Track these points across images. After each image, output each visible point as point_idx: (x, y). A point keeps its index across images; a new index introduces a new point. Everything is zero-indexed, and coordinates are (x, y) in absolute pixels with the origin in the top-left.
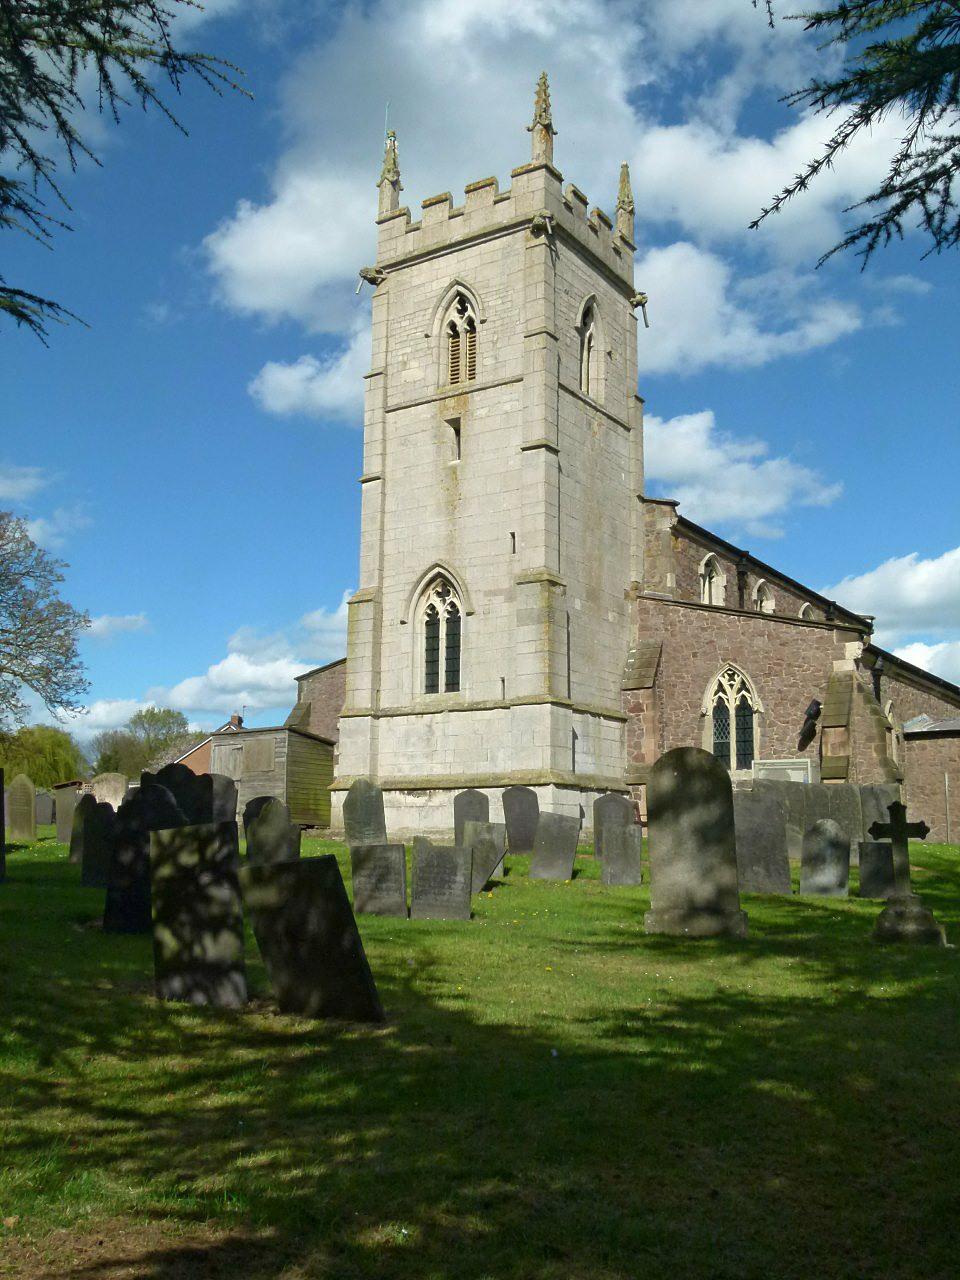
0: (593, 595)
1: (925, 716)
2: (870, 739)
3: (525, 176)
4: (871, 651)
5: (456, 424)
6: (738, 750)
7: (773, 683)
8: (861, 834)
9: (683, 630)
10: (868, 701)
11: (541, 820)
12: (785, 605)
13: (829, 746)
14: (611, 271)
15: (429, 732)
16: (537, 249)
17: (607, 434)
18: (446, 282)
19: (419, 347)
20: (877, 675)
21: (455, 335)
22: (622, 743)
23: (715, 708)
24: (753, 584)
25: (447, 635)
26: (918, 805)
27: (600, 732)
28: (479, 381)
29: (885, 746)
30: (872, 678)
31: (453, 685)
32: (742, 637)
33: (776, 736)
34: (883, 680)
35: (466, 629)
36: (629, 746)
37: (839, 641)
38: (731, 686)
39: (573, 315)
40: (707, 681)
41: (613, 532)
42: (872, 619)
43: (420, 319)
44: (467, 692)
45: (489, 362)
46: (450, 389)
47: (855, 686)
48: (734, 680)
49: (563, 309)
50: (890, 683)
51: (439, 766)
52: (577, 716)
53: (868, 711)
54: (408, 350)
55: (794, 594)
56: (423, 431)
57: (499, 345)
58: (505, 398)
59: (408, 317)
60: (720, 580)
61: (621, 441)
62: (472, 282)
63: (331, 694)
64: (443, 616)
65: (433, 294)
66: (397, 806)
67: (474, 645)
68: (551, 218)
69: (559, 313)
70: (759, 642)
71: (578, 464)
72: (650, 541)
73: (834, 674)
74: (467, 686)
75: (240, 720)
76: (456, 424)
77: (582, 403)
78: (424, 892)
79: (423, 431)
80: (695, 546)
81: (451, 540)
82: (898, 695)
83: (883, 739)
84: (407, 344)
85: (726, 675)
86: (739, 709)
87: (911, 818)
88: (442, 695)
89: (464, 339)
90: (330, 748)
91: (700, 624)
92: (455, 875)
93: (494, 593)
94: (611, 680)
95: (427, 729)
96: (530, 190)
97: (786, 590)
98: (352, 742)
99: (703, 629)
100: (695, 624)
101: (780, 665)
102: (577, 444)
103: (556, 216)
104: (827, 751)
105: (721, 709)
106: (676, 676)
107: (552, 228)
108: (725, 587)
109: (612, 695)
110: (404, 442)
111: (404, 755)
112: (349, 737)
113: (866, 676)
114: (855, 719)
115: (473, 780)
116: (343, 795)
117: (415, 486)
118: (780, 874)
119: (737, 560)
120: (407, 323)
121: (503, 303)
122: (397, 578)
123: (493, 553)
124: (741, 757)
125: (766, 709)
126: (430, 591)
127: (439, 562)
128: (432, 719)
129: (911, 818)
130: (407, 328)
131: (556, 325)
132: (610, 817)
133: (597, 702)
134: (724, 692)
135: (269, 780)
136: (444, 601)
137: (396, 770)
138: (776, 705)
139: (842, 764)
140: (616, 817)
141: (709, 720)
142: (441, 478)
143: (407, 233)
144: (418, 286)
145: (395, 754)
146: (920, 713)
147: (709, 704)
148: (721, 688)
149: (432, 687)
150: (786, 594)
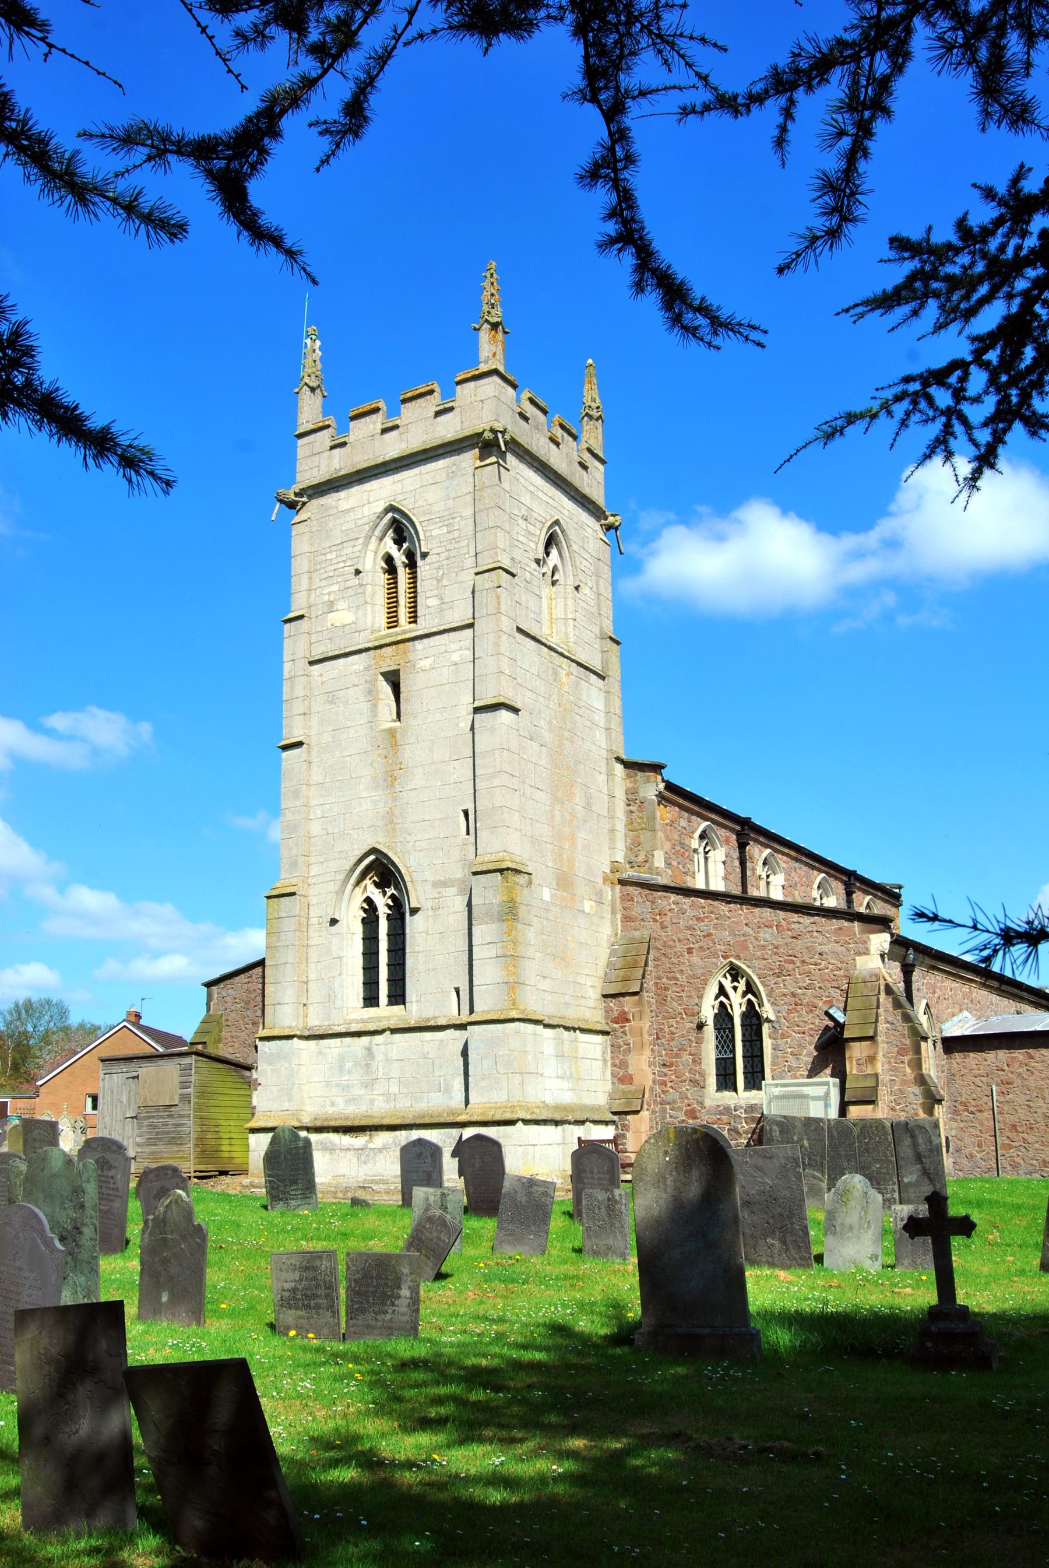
0: (564, 881)
1: (966, 1013)
2: (902, 1052)
3: (472, 384)
4: (900, 943)
5: (394, 680)
6: (745, 1067)
7: (789, 985)
8: (895, 1180)
9: (674, 921)
10: (897, 1005)
11: (506, 1184)
12: (797, 879)
13: (854, 1062)
14: (576, 490)
15: (369, 1055)
16: (489, 468)
17: (578, 685)
18: (381, 506)
19: (349, 584)
20: (907, 971)
21: (391, 568)
22: (605, 1061)
23: (716, 1015)
24: (756, 855)
25: (388, 935)
26: (962, 1125)
27: (577, 1052)
28: (424, 625)
29: (920, 1059)
30: (901, 975)
31: (398, 996)
32: (746, 928)
33: (789, 1050)
34: (917, 975)
35: (410, 930)
36: (614, 1065)
37: (862, 932)
38: (735, 988)
39: (532, 545)
40: (705, 982)
41: (588, 804)
42: (900, 887)
43: (350, 550)
44: (414, 1010)
45: (433, 602)
46: (386, 634)
47: (882, 988)
48: (739, 982)
49: (521, 538)
50: (924, 978)
51: (381, 1098)
52: (549, 1032)
53: (899, 1018)
54: (335, 588)
55: (807, 864)
56: (354, 685)
57: (445, 582)
58: (453, 647)
59: (334, 548)
60: (718, 855)
61: (594, 692)
62: (410, 507)
63: (247, 1003)
64: (383, 911)
65: (364, 521)
66: (330, 1149)
67: (420, 949)
68: (503, 432)
69: (516, 543)
70: (766, 935)
71: (543, 723)
72: (632, 812)
73: (857, 972)
74: (414, 999)
75: (138, 1016)
76: (394, 680)
77: (545, 649)
78: (363, 1311)
79: (354, 685)
80: (686, 815)
81: (390, 820)
82: (934, 992)
83: (918, 1051)
84: (334, 580)
85: (728, 975)
86: (744, 1016)
87: (955, 1210)
88: (385, 1013)
89: (403, 574)
90: (247, 1073)
91: (695, 913)
92: (399, 1287)
93: (444, 884)
94: (589, 983)
95: (364, 1052)
96: (479, 399)
97: (797, 860)
98: (272, 1070)
99: (699, 919)
100: (690, 913)
101: (793, 962)
102: (541, 699)
103: (509, 428)
104: (851, 1068)
105: (723, 1017)
106: (668, 978)
107: (506, 443)
108: (724, 863)
109: (591, 1003)
110: (332, 698)
111: (338, 1085)
112: (270, 1064)
113: (893, 973)
114: (882, 1027)
115: (424, 1116)
116: (266, 1139)
117: (345, 754)
118: (799, 1247)
119: (738, 828)
120: (333, 555)
121: (448, 532)
122: (324, 865)
123: (442, 836)
124: (747, 1044)
125: (777, 1017)
126: (368, 882)
127: (379, 847)
128: (371, 1042)
129: (955, 1210)
130: (333, 562)
131: (513, 559)
132: (592, 1172)
133: (572, 1015)
134: (727, 997)
135: (171, 1116)
136: (384, 893)
137: (328, 1103)
138: (789, 1011)
139: (870, 1083)
140: (598, 1172)
141: (710, 1031)
142: (378, 743)
143: (332, 448)
144: (347, 511)
145: (328, 1084)
146: (961, 1011)
147: (708, 1011)
148: (722, 991)
149: (371, 1000)
150: (797, 865)
